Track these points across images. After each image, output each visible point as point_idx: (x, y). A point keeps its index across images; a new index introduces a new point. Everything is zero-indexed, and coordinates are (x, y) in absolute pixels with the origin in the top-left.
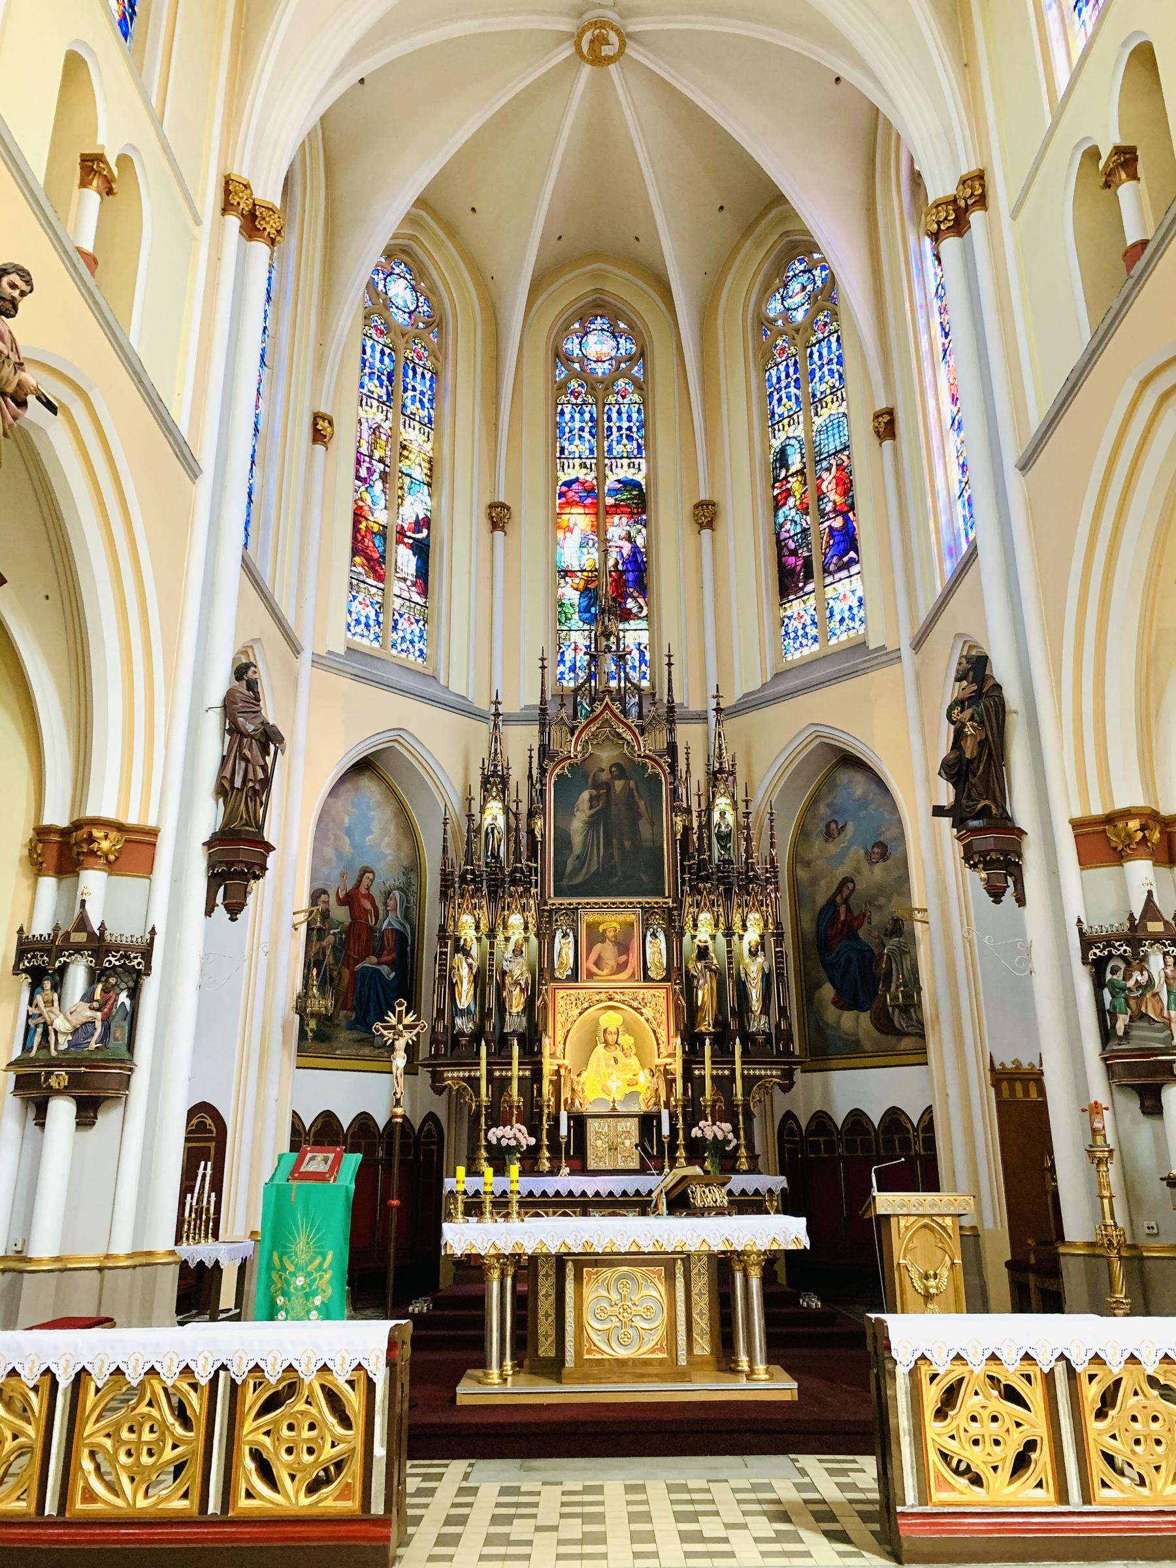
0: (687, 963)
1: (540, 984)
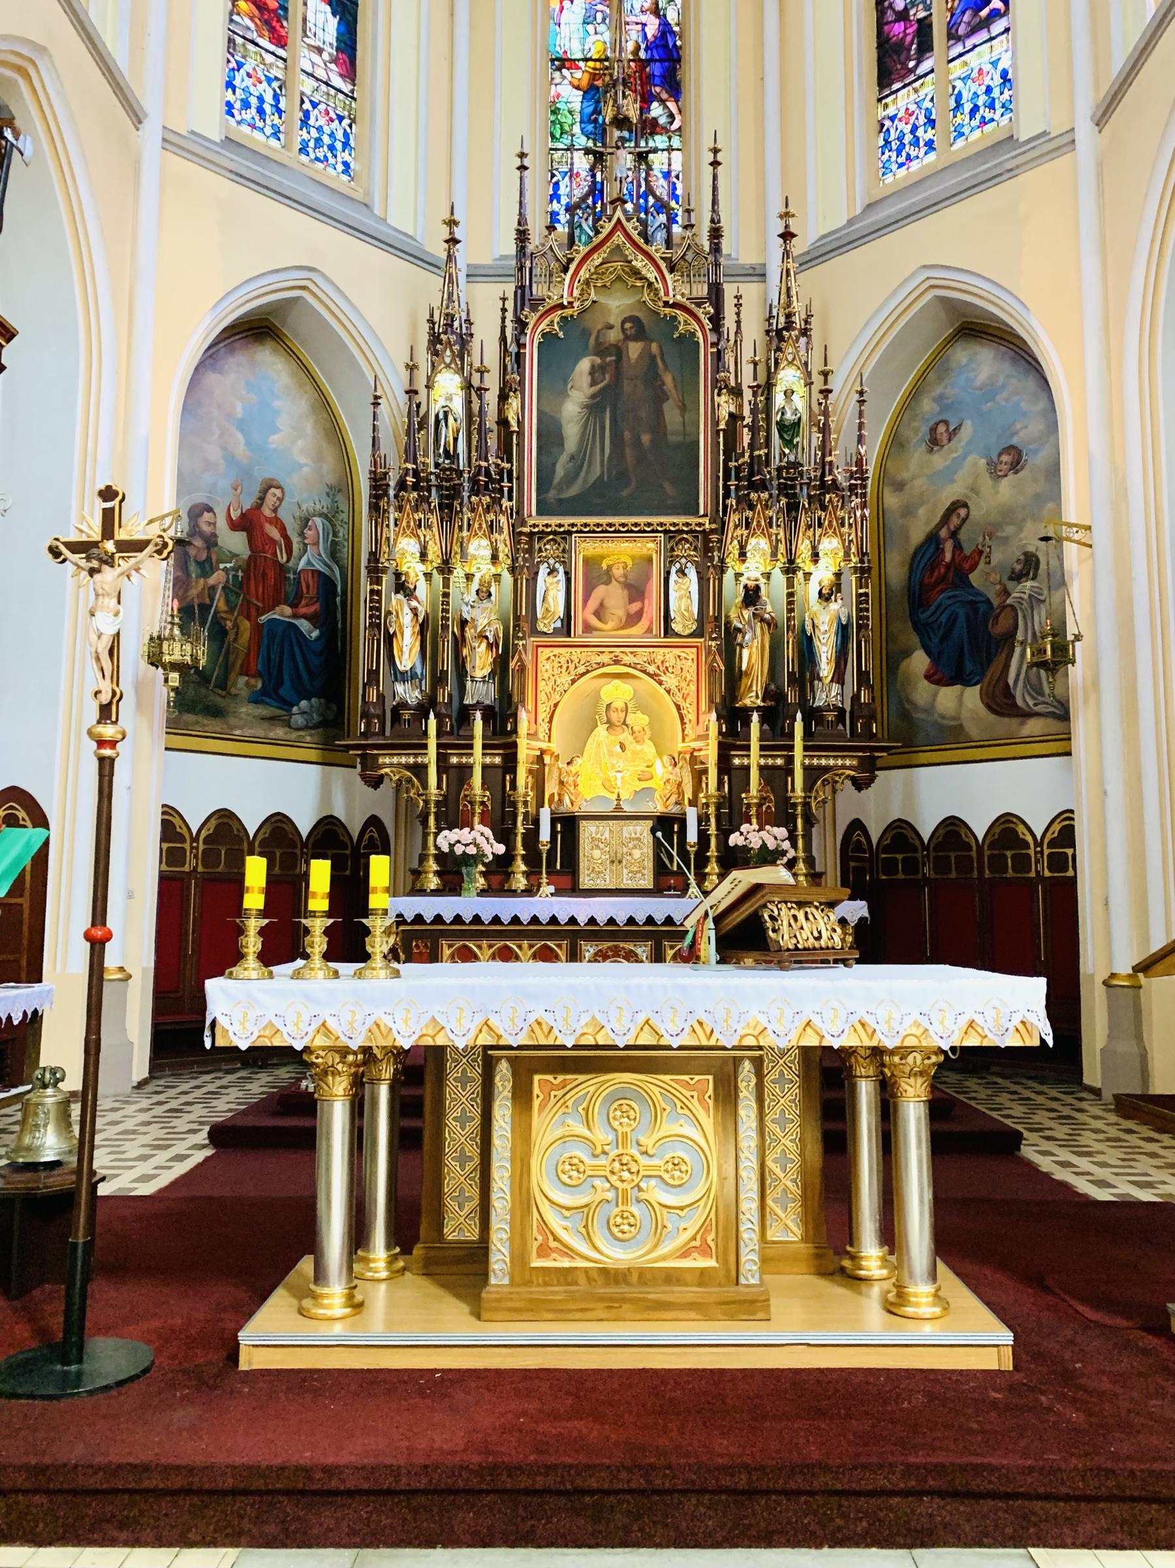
0: (728, 611)
1: (516, 637)
